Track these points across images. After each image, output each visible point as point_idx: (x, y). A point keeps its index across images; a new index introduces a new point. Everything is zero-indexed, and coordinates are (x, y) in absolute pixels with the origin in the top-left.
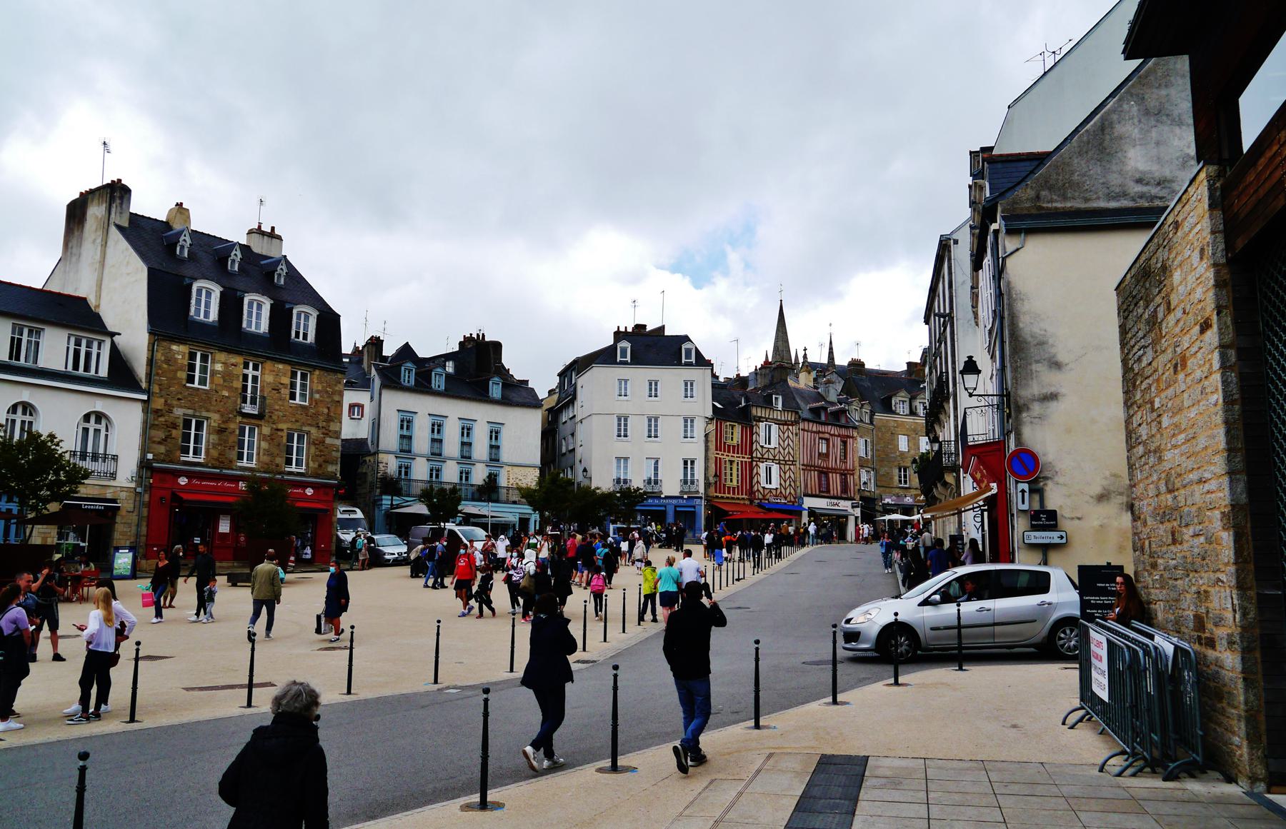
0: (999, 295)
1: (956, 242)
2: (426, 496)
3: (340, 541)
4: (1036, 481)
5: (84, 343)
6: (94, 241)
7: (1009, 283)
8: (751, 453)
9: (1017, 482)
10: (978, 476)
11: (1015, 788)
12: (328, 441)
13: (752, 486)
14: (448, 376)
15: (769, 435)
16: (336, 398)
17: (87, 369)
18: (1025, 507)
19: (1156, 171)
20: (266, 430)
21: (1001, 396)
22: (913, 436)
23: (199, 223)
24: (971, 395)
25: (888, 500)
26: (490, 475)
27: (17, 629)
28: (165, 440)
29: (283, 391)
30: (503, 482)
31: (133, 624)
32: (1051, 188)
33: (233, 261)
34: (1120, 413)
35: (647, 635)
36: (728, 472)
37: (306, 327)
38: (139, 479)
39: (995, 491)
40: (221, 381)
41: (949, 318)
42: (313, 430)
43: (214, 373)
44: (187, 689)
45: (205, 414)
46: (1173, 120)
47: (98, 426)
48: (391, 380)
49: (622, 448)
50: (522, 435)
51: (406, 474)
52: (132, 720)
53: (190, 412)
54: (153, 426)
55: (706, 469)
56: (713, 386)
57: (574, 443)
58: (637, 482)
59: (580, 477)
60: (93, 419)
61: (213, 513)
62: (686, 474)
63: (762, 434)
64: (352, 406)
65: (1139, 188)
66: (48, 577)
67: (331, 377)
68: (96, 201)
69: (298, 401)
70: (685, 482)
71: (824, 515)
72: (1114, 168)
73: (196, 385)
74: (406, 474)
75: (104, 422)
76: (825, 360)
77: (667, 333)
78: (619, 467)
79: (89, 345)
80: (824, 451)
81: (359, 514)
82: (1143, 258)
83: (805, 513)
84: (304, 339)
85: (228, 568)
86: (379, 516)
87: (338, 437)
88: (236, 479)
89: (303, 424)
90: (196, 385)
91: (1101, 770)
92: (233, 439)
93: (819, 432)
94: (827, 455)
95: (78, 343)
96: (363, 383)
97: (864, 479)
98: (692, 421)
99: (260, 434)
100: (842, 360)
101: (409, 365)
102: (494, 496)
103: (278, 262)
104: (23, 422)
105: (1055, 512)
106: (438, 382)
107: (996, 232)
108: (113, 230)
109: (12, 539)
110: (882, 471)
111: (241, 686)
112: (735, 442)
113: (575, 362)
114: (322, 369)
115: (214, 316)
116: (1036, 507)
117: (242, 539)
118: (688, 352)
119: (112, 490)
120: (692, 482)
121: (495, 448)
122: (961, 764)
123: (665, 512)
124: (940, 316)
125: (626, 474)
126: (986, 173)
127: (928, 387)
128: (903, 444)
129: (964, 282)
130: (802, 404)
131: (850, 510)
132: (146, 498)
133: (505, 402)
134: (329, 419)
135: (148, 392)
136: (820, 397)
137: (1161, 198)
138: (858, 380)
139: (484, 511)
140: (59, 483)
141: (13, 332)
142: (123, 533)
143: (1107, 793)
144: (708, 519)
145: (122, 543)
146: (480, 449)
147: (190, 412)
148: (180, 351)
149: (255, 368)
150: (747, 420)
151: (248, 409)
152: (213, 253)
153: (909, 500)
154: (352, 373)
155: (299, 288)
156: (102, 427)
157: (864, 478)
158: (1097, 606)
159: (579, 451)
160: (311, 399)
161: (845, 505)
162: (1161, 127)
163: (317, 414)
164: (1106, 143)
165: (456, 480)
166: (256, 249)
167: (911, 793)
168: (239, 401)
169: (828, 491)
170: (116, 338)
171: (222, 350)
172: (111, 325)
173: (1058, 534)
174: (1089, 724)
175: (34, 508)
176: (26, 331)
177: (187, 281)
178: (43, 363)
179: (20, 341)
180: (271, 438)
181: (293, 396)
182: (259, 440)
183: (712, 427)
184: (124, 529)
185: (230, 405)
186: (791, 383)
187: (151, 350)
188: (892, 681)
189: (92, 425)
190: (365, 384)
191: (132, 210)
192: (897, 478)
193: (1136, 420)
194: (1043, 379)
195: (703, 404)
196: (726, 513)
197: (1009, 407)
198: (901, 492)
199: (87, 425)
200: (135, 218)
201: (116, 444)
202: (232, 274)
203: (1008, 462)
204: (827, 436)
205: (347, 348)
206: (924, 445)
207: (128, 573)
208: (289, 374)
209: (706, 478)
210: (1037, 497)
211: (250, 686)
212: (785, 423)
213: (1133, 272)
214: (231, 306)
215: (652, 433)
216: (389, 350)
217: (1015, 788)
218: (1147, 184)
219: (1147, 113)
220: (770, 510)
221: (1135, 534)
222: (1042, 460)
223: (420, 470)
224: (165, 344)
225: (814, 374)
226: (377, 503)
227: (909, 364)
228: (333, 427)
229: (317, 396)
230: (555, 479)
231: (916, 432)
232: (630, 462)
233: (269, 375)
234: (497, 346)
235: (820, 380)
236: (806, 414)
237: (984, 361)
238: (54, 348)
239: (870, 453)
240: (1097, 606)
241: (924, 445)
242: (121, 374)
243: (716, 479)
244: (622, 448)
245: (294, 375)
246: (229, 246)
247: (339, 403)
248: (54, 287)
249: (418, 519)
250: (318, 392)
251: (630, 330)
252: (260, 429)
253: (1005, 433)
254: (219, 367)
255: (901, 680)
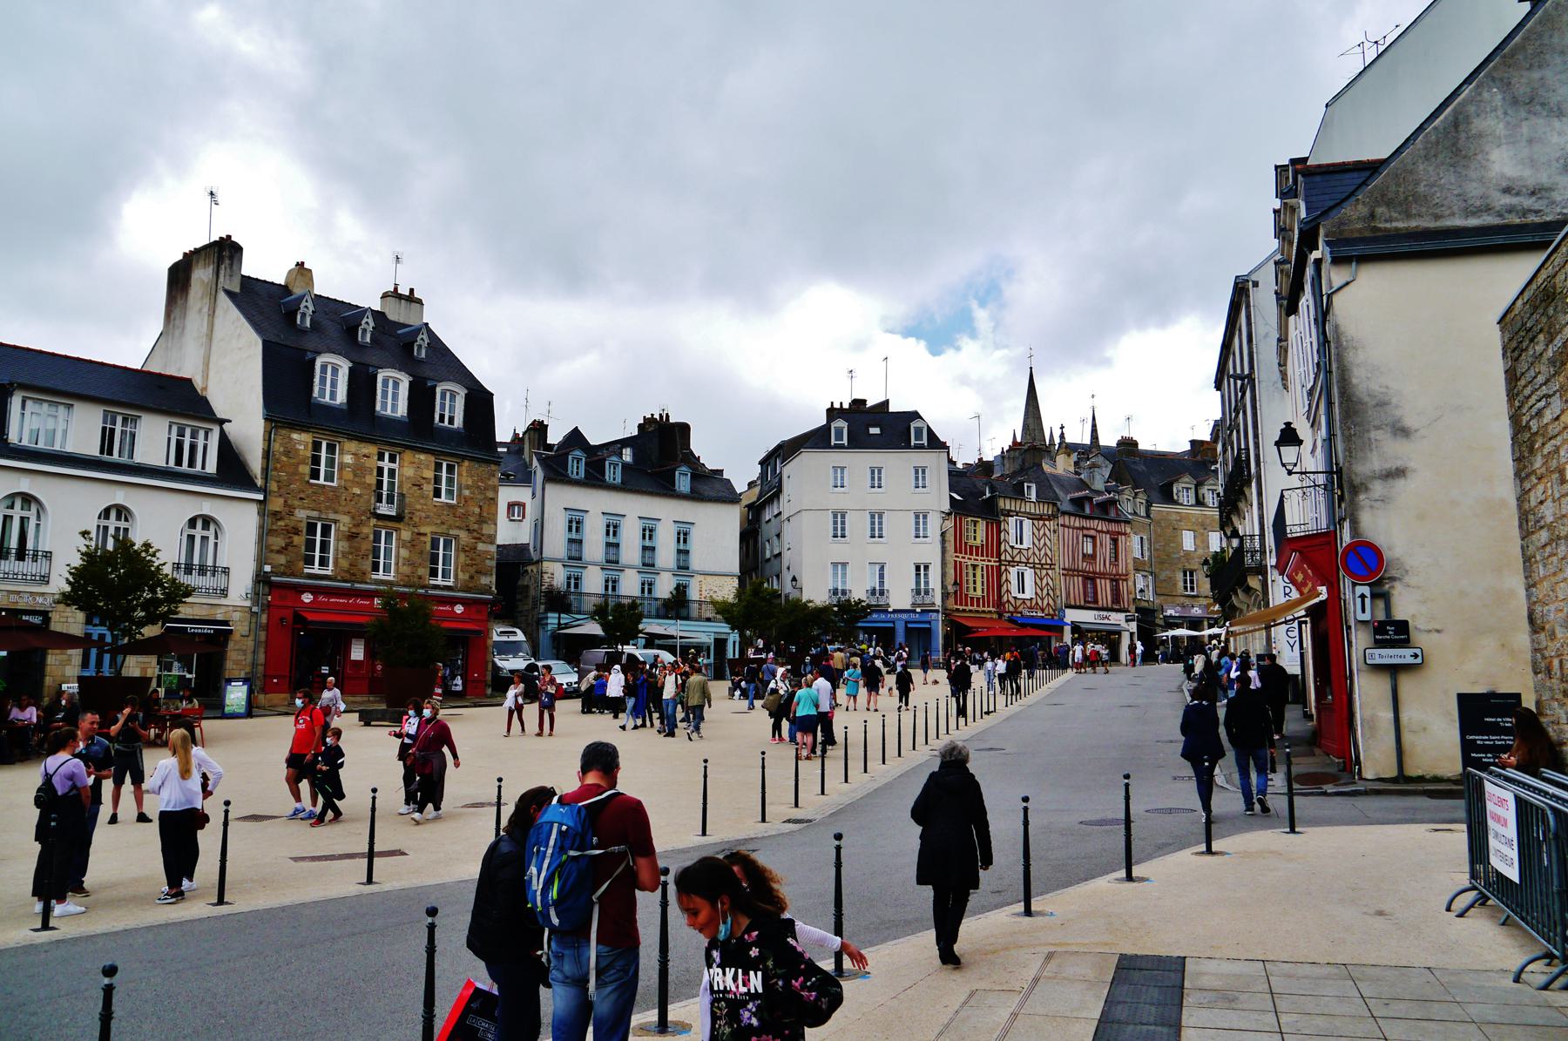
0: (1324, 342)
1: (1256, 284)
2: (600, 613)
3: (496, 669)
4: (1380, 582)
5: (188, 432)
6: (200, 310)
7: (1337, 327)
8: (999, 555)
9: (1354, 585)
10: (1300, 577)
11: (1398, 1008)
12: (481, 547)
13: (1000, 596)
14: (625, 466)
15: (1021, 533)
16: (490, 494)
17: (192, 463)
18: (1367, 617)
19: (1529, 177)
20: (406, 535)
21: (1329, 473)
22: (1201, 529)
23: (325, 286)
24: (1290, 473)
25: (1170, 612)
26: (678, 586)
27: (74, 787)
28: (285, 548)
29: (425, 487)
30: (693, 594)
31: (220, 776)
32: (1389, 204)
33: (365, 331)
34: (1506, 490)
35: (876, 786)
36: (971, 578)
37: (452, 408)
38: (256, 596)
39: (1324, 597)
40: (350, 476)
41: (1249, 380)
42: (463, 535)
43: (342, 466)
44: (296, 859)
45: (332, 516)
46: (1551, 110)
47: (205, 533)
48: (557, 472)
49: (839, 551)
50: (716, 537)
51: (576, 586)
52: (221, 901)
53: (315, 514)
54: (271, 532)
55: (944, 575)
56: (950, 473)
57: (781, 546)
58: (858, 593)
59: (788, 588)
60: (199, 524)
61: (342, 637)
62: (918, 583)
63: (1012, 531)
64: (511, 506)
65: (1507, 200)
66: (130, 718)
67: (483, 469)
68: (201, 263)
69: (443, 499)
70: (918, 592)
71: (1091, 631)
72: (1473, 175)
73: (321, 481)
74: (576, 586)
75: (212, 527)
76: (1087, 441)
77: (892, 409)
78: (835, 575)
79: (194, 435)
80: (1090, 551)
81: (520, 636)
82: (1543, 275)
83: (1067, 629)
84: (456, 427)
85: (362, 703)
86: (544, 638)
87: (492, 543)
88: (370, 595)
89: (451, 527)
90: (321, 481)
91: (1517, 980)
92: (366, 546)
93: (1083, 528)
94: (1093, 556)
95: (181, 434)
96: (523, 477)
97: (1140, 585)
98: (925, 517)
99: (398, 539)
100: (1108, 439)
101: (578, 453)
102: (683, 612)
103: (418, 331)
104: (117, 529)
105: (1406, 623)
106: (613, 474)
107: (1318, 262)
108: (222, 296)
109: (107, 671)
110: (1163, 576)
111: (490, 804)
112: (978, 542)
113: (779, 447)
114: (472, 459)
115: (341, 397)
116: (1381, 616)
117: (379, 667)
118: (919, 431)
119: (223, 610)
120: (927, 592)
121: (683, 553)
122: (1316, 970)
123: (893, 629)
124: (1236, 377)
125: (844, 582)
126: (1301, 188)
127: (1222, 468)
128: (1188, 541)
129: (1266, 335)
130: (1061, 494)
131: (1124, 624)
132: (264, 619)
133: (695, 496)
134: (482, 520)
135: (264, 490)
136: (1083, 485)
137: (1537, 212)
138: (1129, 461)
139: (671, 631)
140: (155, 602)
141: (105, 422)
142: (237, 663)
143: (1534, 1015)
144: (947, 637)
145: (236, 674)
146: (666, 555)
147: (315, 514)
148: (302, 440)
149: (392, 460)
150: (992, 513)
151: (384, 509)
152: (340, 321)
153: (1197, 611)
154: (510, 465)
155: (444, 362)
156: (211, 534)
157: (1140, 584)
158: (1485, 749)
159: (786, 556)
160: (459, 495)
161: (1117, 618)
162: (1534, 120)
163: (466, 515)
164: (1461, 143)
165: (637, 592)
166: (392, 317)
167: (1254, 1016)
168: (373, 500)
169: (1096, 601)
170: (226, 426)
171: (352, 438)
172: (220, 411)
173: (1411, 651)
174: (1483, 910)
175: (127, 632)
176: (119, 420)
177: (310, 355)
178: (139, 458)
179: (112, 431)
180: (412, 545)
181: (437, 493)
182: (398, 547)
183: (950, 524)
184: (238, 657)
185: (362, 505)
186: (1047, 468)
187: (268, 440)
188: (1203, 848)
189: (198, 532)
190: (525, 478)
191: (245, 272)
192: (1181, 584)
193: (1534, 498)
194: (1384, 451)
195: (938, 496)
196: (969, 630)
197: (1341, 486)
198: (1187, 602)
199: (192, 532)
200: (248, 282)
201: (223, 555)
202: (363, 347)
203: (1339, 559)
204: (1092, 533)
205: (503, 434)
206: (1215, 542)
207: (242, 711)
208: (433, 466)
209: (944, 587)
210: (1381, 604)
211: (371, 855)
212: (1041, 518)
213: (1526, 296)
214: (362, 385)
215: (876, 533)
216: (555, 437)
217: (1398, 1008)
218: (1518, 194)
219: (1515, 102)
220: (1023, 626)
221: (1536, 650)
222: (1386, 555)
223: (593, 582)
224: (283, 432)
225: (1074, 457)
226: (541, 622)
227: (1193, 442)
228: (487, 529)
229: (467, 493)
230: (757, 590)
231: (1204, 526)
232: (832, 483)
233: (411, 467)
234: (684, 429)
235: (1082, 464)
236: (1066, 506)
237: (1303, 429)
238: (153, 439)
239: (1146, 554)
240: (1485, 749)
241: (1215, 542)
242: (232, 469)
243: (956, 589)
244: (839, 551)
245: (438, 467)
246: (361, 312)
247: (493, 501)
248: (155, 368)
249: (591, 641)
250: (468, 487)
251: (846, 406)
252: (403, 533)
253: (1335, 521)
254: (348, 459)
255: (1215, 846)
